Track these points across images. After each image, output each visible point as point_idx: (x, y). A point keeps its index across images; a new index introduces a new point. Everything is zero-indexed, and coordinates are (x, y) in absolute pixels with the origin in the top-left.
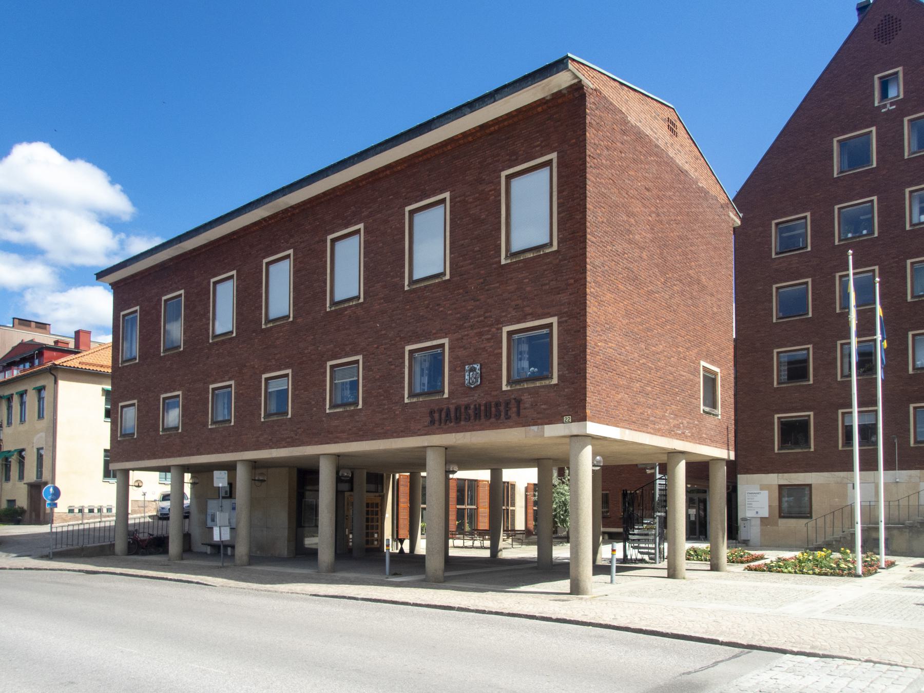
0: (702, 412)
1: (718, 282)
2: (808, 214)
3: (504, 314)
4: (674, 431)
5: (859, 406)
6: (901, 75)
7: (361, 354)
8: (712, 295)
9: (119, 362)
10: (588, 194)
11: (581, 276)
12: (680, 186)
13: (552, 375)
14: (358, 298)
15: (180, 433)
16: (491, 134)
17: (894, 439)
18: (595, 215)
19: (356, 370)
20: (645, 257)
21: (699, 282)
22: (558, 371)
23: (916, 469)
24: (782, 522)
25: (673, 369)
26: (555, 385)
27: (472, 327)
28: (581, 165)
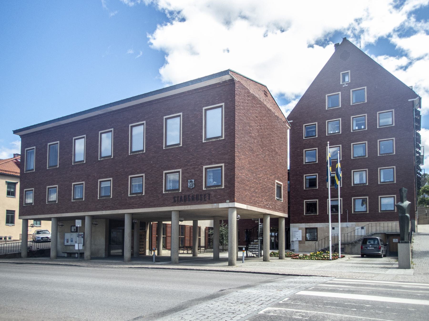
0: (276, 199)
1: (282, 151)
2: (317, 123)
3: (204, 161)
5: (331, 198)
8: (280, 155)
9: (24, 171)
10: (236, 119)
11: (233, 149)
14: (143, 151)
15: (57, 203)
20: (256, 142)
21: (275, 151)
23: (354, 222)
24: (307, 242)
25: (265, 183)
26: (223, 189)
27: (191, 165)
28: (233, 109)
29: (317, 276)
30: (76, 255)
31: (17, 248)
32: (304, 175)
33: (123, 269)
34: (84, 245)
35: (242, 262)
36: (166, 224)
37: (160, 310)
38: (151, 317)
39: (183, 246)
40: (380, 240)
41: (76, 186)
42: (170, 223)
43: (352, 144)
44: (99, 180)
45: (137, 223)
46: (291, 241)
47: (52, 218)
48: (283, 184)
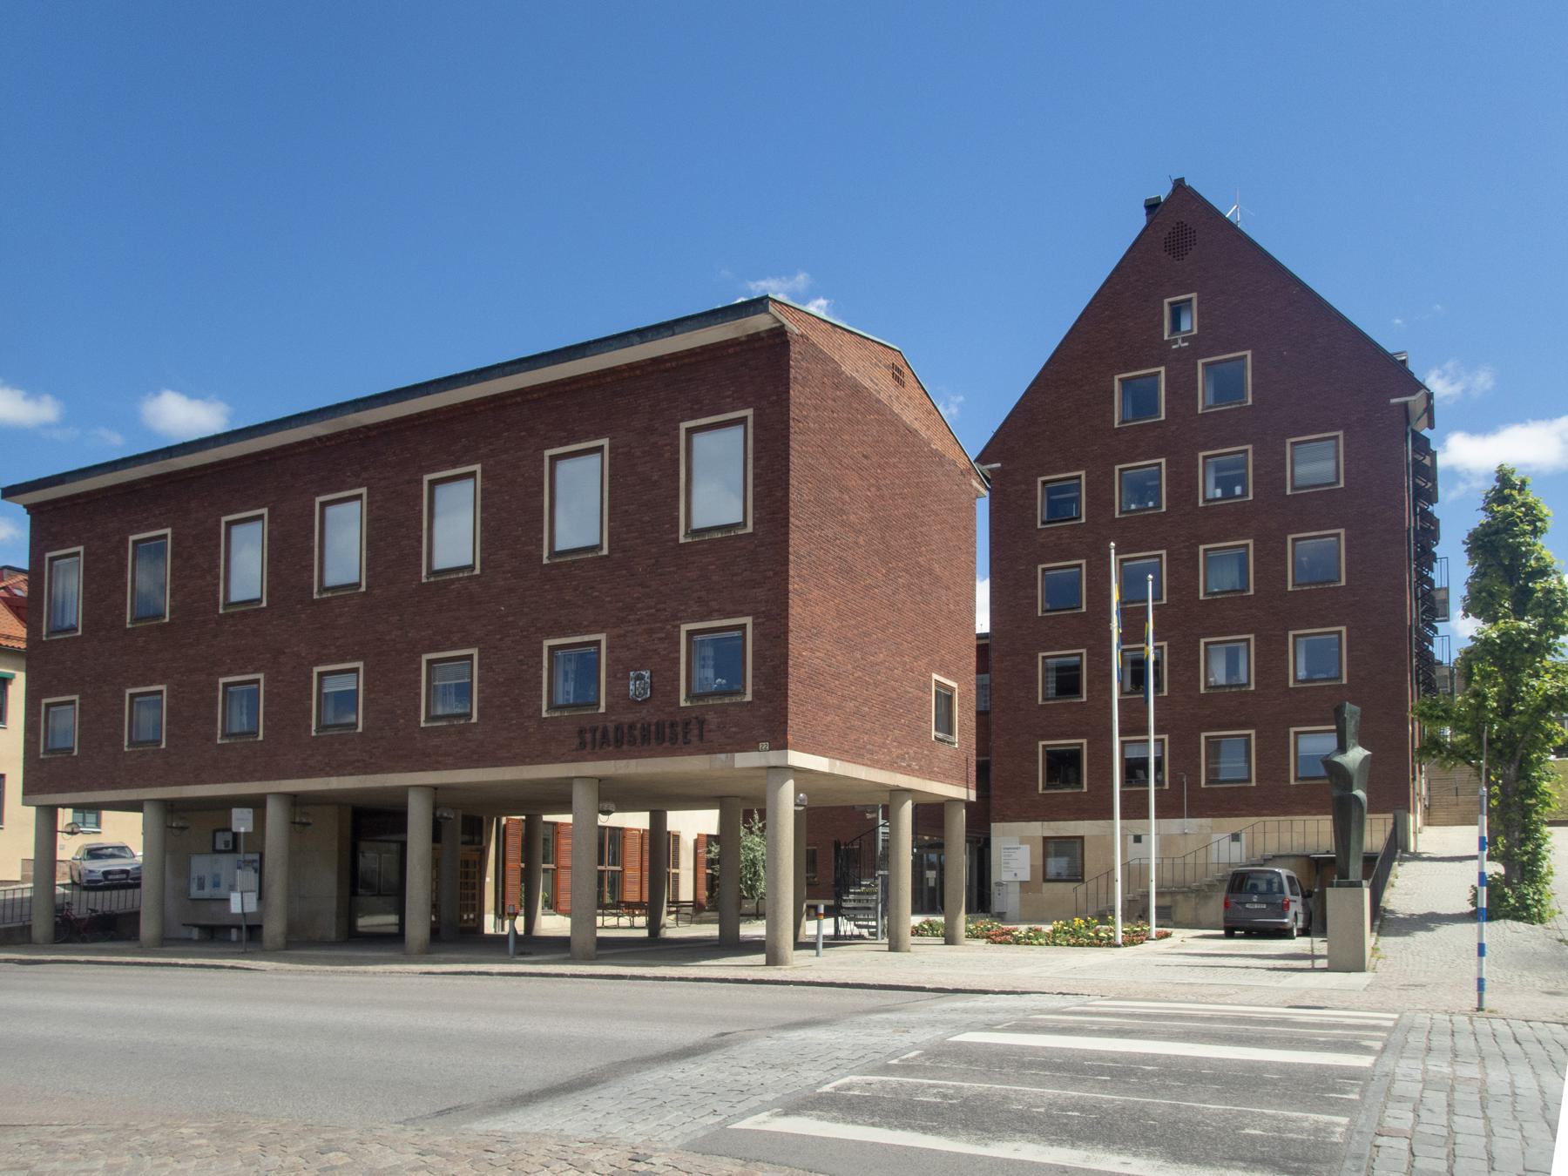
0: (933, 739)
1: (956, 571)
3: (682, 608)
4: (896, 763)
5: (1121, 735)
6: (1195, 304)
7: (475, 647)
8: (947, 588)
9: (42, 632)
12: (908, 450)
13: (745, 690)
14: (472, 567)
15: (163, 749)
16: (667, 370)
17: (1182, 777)
18: (800, 491)
19: (467, 670)
20: (862, 543)
21: (930, 571)
22: (753, 685)
23: (1208, 816)
26: (749, 703)
27: (639, 621)
28: (783, 430)
29: (1045, 993)
30: (234, 934)
31: (17, 911)
32: (1041, 655)
33: (400, 977)
34: (260, 898)
35: (814, 952)
36: (555, 824)
37: (519, 1090)
38: (490, 1107)
39: (610, 897)
40: (1290, 879)
41: (231, 689)
42: (566, 818)
43: (1202, 548)
44: (316, 670)
45: (450, 819)
46: (993, 882)
47: (268, 796)
48: (962, 686)
